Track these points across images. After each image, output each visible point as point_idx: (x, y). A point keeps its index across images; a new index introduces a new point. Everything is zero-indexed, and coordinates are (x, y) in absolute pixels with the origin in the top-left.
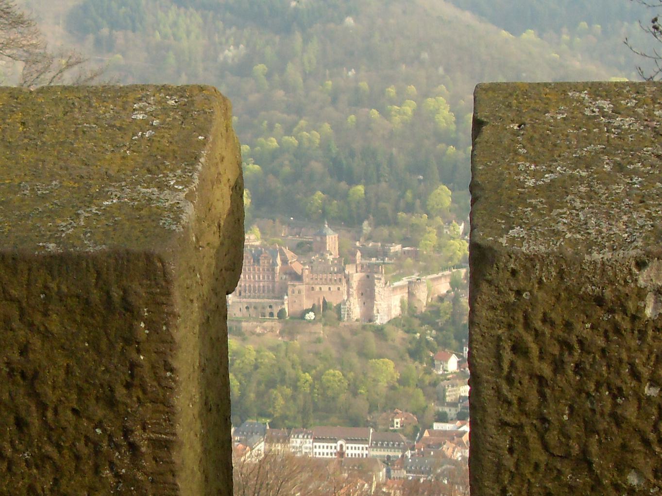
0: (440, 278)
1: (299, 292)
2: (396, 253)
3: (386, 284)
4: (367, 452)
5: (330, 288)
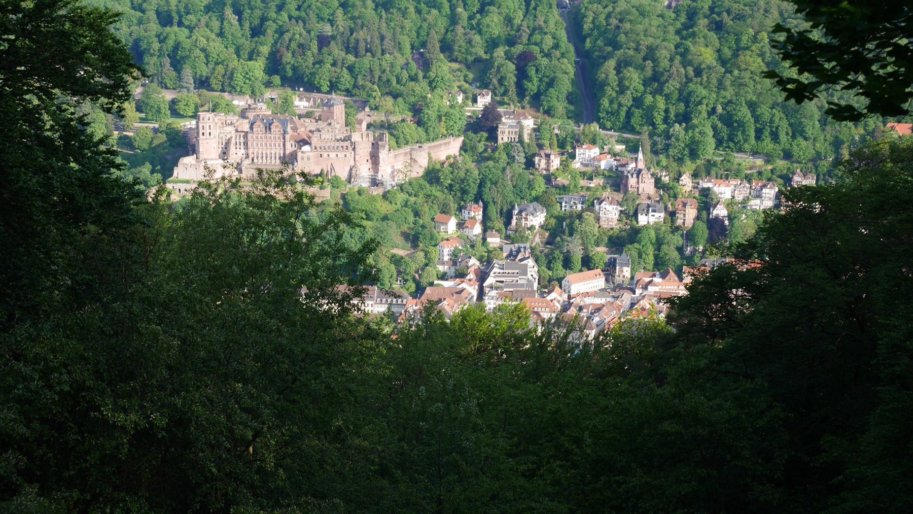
0: (441, 145)
1: (309, 159)
2: (65, 25)
3: (390, 150)
4: (372, 309)
5: (337, 155)
